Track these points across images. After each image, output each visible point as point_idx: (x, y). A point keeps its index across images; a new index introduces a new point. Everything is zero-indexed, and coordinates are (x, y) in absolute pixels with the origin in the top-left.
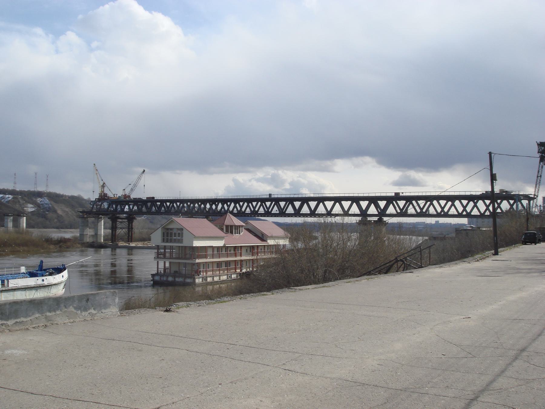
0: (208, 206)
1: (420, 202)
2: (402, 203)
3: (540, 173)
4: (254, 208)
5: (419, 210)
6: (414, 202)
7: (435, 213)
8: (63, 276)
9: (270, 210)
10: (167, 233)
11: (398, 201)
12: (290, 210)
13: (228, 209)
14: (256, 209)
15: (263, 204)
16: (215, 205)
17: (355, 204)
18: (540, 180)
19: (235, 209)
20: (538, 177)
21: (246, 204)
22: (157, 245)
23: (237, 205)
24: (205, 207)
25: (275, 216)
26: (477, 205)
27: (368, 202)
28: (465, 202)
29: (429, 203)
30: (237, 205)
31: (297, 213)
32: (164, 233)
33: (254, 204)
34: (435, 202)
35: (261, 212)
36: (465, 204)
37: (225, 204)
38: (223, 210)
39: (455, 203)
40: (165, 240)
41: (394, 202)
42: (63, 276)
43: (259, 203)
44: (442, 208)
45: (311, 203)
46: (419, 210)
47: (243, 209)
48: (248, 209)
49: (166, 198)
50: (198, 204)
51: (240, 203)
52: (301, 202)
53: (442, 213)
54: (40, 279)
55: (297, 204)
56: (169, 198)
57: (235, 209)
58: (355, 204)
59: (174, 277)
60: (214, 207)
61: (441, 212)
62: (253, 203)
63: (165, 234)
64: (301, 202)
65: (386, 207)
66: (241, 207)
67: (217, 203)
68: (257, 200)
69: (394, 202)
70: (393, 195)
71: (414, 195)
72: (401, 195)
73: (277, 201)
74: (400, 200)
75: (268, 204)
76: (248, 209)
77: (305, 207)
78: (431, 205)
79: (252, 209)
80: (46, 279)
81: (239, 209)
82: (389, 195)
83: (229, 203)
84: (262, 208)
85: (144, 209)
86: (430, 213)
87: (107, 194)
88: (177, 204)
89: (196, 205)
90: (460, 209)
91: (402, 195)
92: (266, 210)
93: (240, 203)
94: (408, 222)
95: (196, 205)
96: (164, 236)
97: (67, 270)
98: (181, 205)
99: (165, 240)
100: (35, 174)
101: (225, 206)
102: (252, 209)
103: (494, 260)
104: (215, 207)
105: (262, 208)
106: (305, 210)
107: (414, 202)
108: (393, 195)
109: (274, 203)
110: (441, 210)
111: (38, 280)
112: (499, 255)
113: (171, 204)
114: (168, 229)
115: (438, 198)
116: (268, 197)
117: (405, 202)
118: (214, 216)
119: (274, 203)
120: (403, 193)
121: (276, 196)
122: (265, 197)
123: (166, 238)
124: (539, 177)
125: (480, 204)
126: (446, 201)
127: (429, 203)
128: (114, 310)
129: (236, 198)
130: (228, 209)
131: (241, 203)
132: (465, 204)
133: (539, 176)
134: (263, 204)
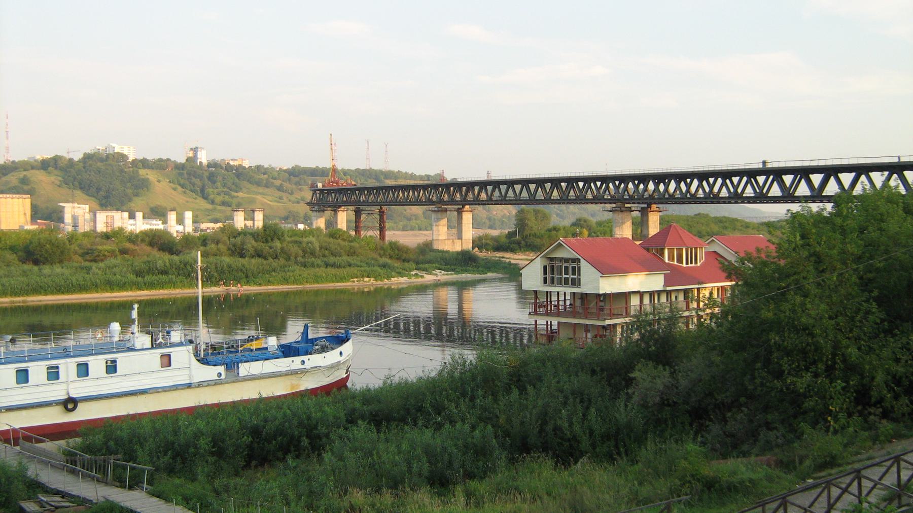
0: (651, 186)
4: (736, 187)
8: (341, 353)
9: (765, 191)
10: (553, 268)
12: (803, 189)
13: (688, 190)
14: (739, 190)
19: (700, 191)
21: (720, 181)
22: (534, 291)
23: (705, 183)
24: (646, 189)
25: (775, 202)
30: (681, 185)
32: (545, 268)
35: (748, 195)
37: (683, 182)
38: (678, 192)
40: (549, 280)
42: (341, 353)
43: (745, 179)
45: (842, 176)
48: (724, 190)
49: (577, 175)
50: (634, 183)
51: (710, 179)
54: (298, 360)
55: (788, 179)
56: (581, 174)
57: (700, 191)
60: (662, 187)
63: (549, 270)
66: (711, 187)
67: (667, 181)
68: (740, 173)
73: (778, 174)
75: (761, 179)
76: (724, 190)
79: (732, 190)
80: (309, 359)
81: (707, 189)
83: (688, 180)
84: (749, 188)
85: (525, 194)
88: (596, 185)
89: (630, 185)
92: (758, 191)
93: (710, 179)
95: (630, 185)
96: (545, 273)
97: (350, 341)
98: (623, 185)
99: (549, 280)
100: (366, 142)
101: (683, 185)
102: (732, 190)
105: (749, 188)
106: (803, 189)
109: (771, 177)
111: (293, 361)
113: (604, 185)
114: (552, 259)
116: (761, 166)
118: (662, 203)
119: (771, 177)
121: (775, 165)
123: (549, 276)
130: (688, 190)
131: (617, 183)
134: (752, 179)
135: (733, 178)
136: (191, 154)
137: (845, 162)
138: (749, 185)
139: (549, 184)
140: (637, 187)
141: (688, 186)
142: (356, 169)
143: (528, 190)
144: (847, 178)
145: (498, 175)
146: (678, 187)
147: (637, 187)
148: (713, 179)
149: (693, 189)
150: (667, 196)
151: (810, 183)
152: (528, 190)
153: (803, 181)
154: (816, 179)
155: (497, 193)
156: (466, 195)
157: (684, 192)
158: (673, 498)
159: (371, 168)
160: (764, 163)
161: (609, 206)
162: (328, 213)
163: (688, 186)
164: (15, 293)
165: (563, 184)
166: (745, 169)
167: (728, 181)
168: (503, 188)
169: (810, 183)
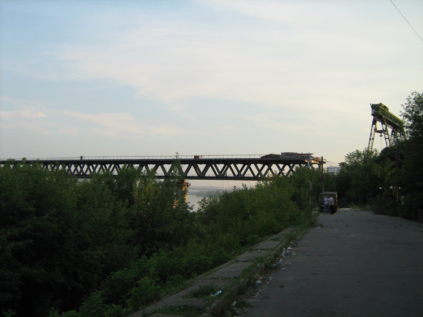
0: (73, 168)
2: (220, 167)
3: (372, 135)
5: (236, 173)
6: (232, 166)
7: (252, 176)
11: (279, 164)
15: (117, 166)
16: (69, 166)
18: (373, 143)
20: (370, 139)
21: (99, 166)
23: (91, 167)
24: (70, 169)
26: (289, 169)
27: (205, 165)
28: (260, 166)
29: (246, 166)
30: (78, 168)
31: (221, 176)
33: (108, 166)
36: (239, 170)
41: (213, 165)
43: (113, 165)
44: (239, 172)
45: (165, 166)
46: (236, 173)
47: (97, 170)
52: (96, 165)
53: (260, 176)
61: (258, 174)
62: (106, 165)
64: (96, 165)
65: (206, 169)
66: (94, 169)
67: (70, 165)
69: (213, 165)
70: (193, 158)
71: (131, 159)
72: (200, 158)
74: (219, 164)
77: (192, 170)
81: (92, 170)
82: (137, 159)
83: (82, 165)
86: (227, 176)
87: (357, 151)
90: (256, 172)
91: (201, 158)
104: (80, 169)
107: (232, 166)
108: (193, 158)
110: (258, 172)
112: (337, 213)
115: (236, 161)
116: (80, 159)
117: (223, 165)
120: (202, 156)
122: (77, 159)
124: (372, 140)
126: (224, 165)
129: (66, 160)
131: (94, 166)
133: (371, 138)
134: (117, 166)
136: (345, 157)
137: (123, 158)
140: (64, 168)
141: (82, 169)
142: (341, 163)
144: (151, 166)
146: (76, 169)
147: (64, 168)
148: (109, 165)
150: (82, 174)
157: (79, 171)
159: (174, 158)
160: (81, 157)
163: (82, 169)
166: (72, 160)
167: (103, 166)
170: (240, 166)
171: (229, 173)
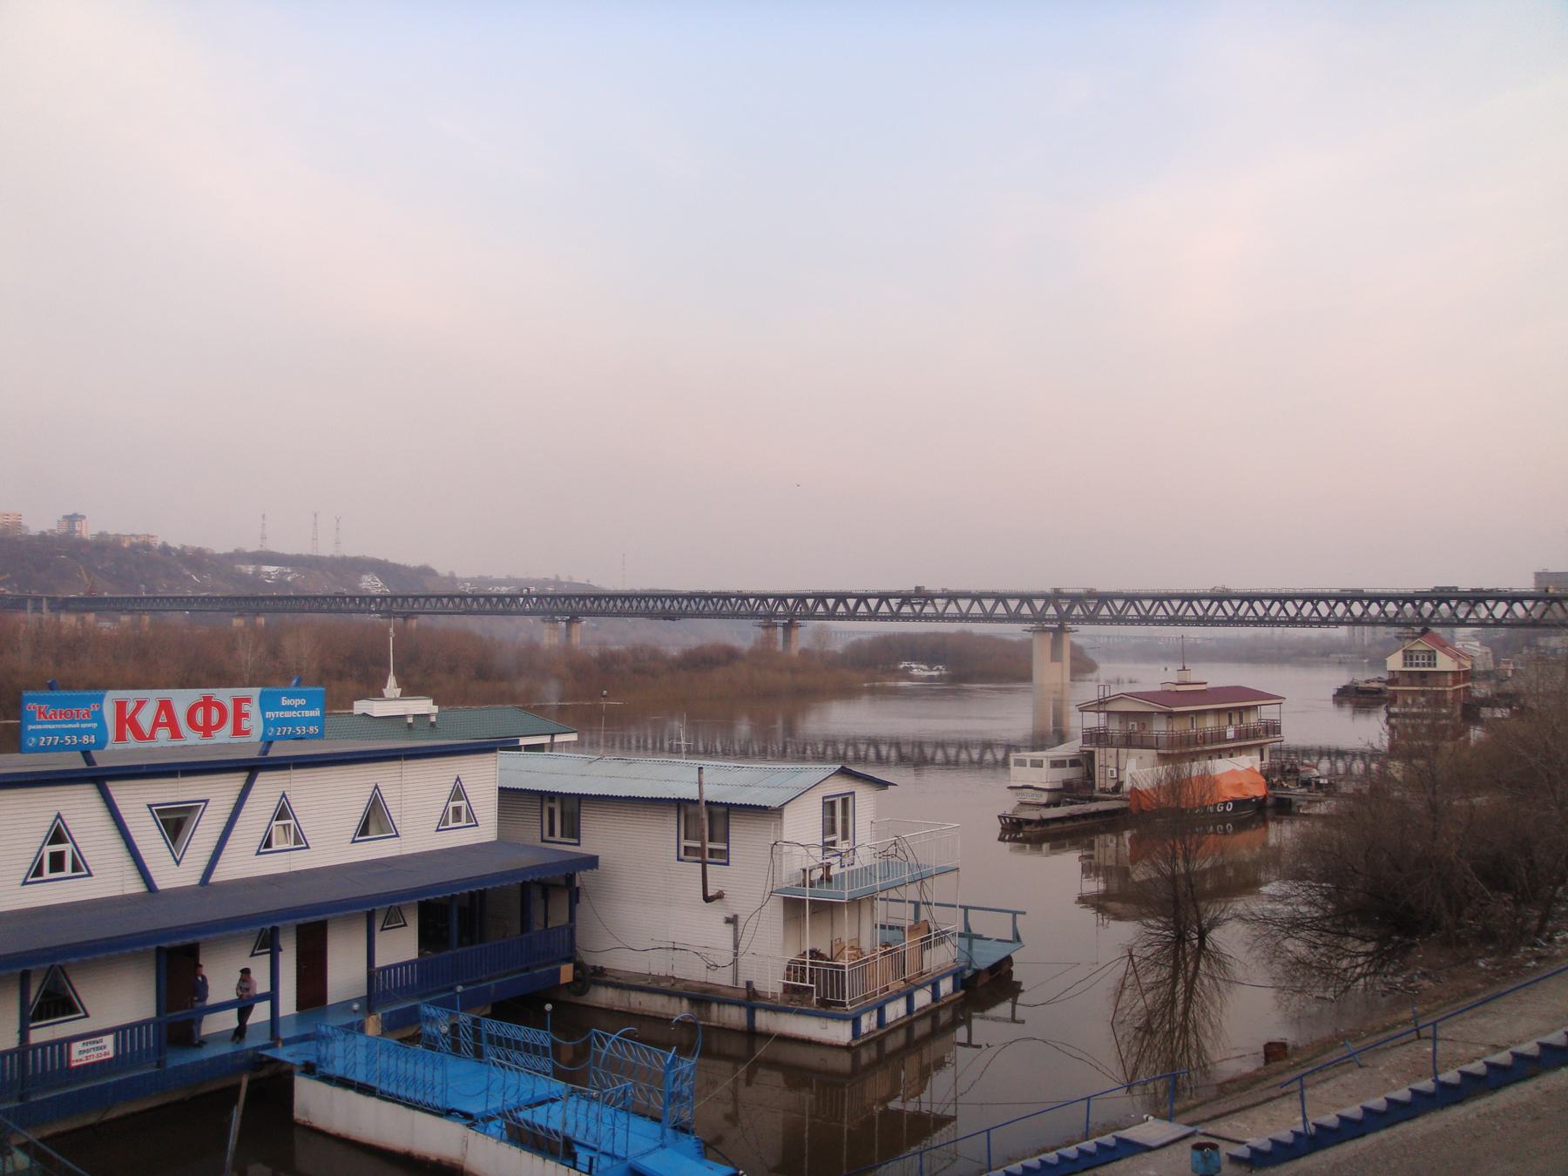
1: (1144, 602)
2: (1119, 604)
6: (1137, 602)
14: (718, 608)
17: (976, 603)
28: (1236, 603)
34: (1195, 603)
39: (1286, 606)
45: (960, 602)
48: (724, 609)
55: (873, 603)
58: (976, 603)
59: (1179, 751)
78: (839, 604)
85: (475, 606)
89: (659, 603)
90: (1230, 612)
94: (940, 630)
103: (1008, 1123)
125: (1289, 605)
127: (1186, 603)
128: (963, 1127)
130: (680, 608)
132: (1490, 607)
135: (750, 600)
138: (1190, 608)
139: (833, 600)
143: (454, 603)
145: (709, 588)
149: (684, 606)
151: (868, 605)
152: (454, 603)
153: (1105, 606)
154: (830, 602)
155: (428, 606)
156: (391, 605)
158: (614, 1085)
161: (1028, 626)
162: (1546, 639)
164: (848, 1110)
165: (378, 600)
166: (1375, 594)
168: (433, 600)
169: (826, 605)
170: (1176, 604)
171: (873, 603)
